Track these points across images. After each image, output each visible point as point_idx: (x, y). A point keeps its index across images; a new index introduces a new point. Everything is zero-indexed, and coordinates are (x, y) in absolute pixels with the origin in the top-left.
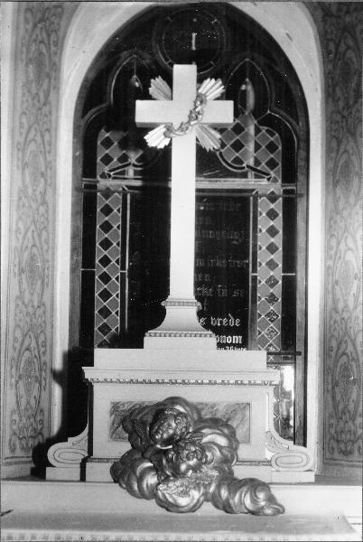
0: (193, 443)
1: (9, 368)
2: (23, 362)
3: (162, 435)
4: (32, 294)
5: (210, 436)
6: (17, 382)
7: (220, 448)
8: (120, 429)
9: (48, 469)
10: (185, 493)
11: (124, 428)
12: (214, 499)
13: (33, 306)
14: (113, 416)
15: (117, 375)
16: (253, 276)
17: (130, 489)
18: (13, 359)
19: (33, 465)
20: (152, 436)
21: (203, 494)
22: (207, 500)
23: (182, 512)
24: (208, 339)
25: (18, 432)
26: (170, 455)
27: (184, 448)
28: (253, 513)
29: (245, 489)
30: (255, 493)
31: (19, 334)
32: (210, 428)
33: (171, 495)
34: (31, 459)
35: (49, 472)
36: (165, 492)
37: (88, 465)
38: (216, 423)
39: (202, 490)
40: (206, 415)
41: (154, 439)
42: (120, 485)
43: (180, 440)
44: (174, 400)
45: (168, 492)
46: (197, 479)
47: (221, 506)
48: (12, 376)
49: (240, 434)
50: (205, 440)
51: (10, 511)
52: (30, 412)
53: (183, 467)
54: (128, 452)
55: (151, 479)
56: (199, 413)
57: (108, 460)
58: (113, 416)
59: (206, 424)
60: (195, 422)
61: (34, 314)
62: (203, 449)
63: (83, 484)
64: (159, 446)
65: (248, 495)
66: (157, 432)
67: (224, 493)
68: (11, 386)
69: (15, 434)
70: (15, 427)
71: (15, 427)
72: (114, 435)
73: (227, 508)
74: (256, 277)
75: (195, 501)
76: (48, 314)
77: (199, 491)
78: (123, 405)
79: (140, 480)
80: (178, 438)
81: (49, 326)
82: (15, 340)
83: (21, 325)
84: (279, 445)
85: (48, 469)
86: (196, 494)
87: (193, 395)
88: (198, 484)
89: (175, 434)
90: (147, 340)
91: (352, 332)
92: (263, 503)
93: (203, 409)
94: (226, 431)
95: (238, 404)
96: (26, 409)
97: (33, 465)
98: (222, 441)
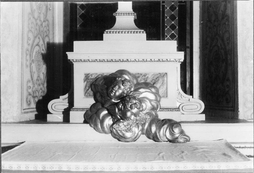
0: (134, 98)
1: (25, 55)
2: (34, 53)
3: (115, 93)
4: (40, 13)
5: (145, 94)
6: (31, 64)
7: (150, 101)
8: (90, 90)
9: (48, 115)
10: (129, 130)
11: (92, 90)
12: (148, 134)
13: (40, 20)
14: (86, 82)
15: (89, 58)
16: (162, 5)
17: (96, 128)
18: (28, 50)
19: (36, 113)
20: (108, 95)
21: (141, 130)
22: (143, 134)
23: (128, 142)
24: (141, 34)
25: (32, 93)
26: (120, 106)
27: (128, 102)
28: (170, 141)
29: (166, 126)
30: (172, 129)
31: (31, 35)
32: (144, 88)
33: (121, 131)
34: (35, 109)
35: (49, 118)
36: (117, 129)
37: (72, 113)
38: (147, 85)
39: (140, 127)
40: (141, 80)
41: (110, 98)
42: (90, 125)
43: (126, 96)
44: (121, 72)
45: (119, 129)
46: (137, 120)
47: (151, 137)
48: (27, 60)
49: (161, 92)
50: (141, 96)
51: (23, 143)
52: (40, 82)
53: (129, 114)
54: (93, 106)
55: (109, 121)
56: (137, 80)
57: (82, 109)
58: (86, 82)
59: (141, 86)
60: (135, 85)
61: (42, 25)
62: (141, 101)
63: (66, 125)
64: (113, 100)
65: (168, 130)
66: (112, 91)
67: (154, 129)
68: (27, 66)
69: (30, 94)
70: (30, 91)
71: (30, 91)
72: (86, 94)
73: (155, 138)
74: (164, 5)
75: (136, 135)
76: (51, 26)
77: (138, 127)
78: (92, 75)
79: (102, 122)
80: (125, 95)
81: (51, 32)
82: (29, 39)
83: (33, 30)
84: (184, 98)
85: (49, 116)
86: (136, 130)
87: (132, 68)
88: (137, 124)
89: (123, 92)
90: (105, 35)
91: (221, 32)
92: (177, 135)
93: (139, 77)
94: (153, 90)
95: (160, 74)
96: (37, 80)
97: (36, 113)
98: (152, 97)
